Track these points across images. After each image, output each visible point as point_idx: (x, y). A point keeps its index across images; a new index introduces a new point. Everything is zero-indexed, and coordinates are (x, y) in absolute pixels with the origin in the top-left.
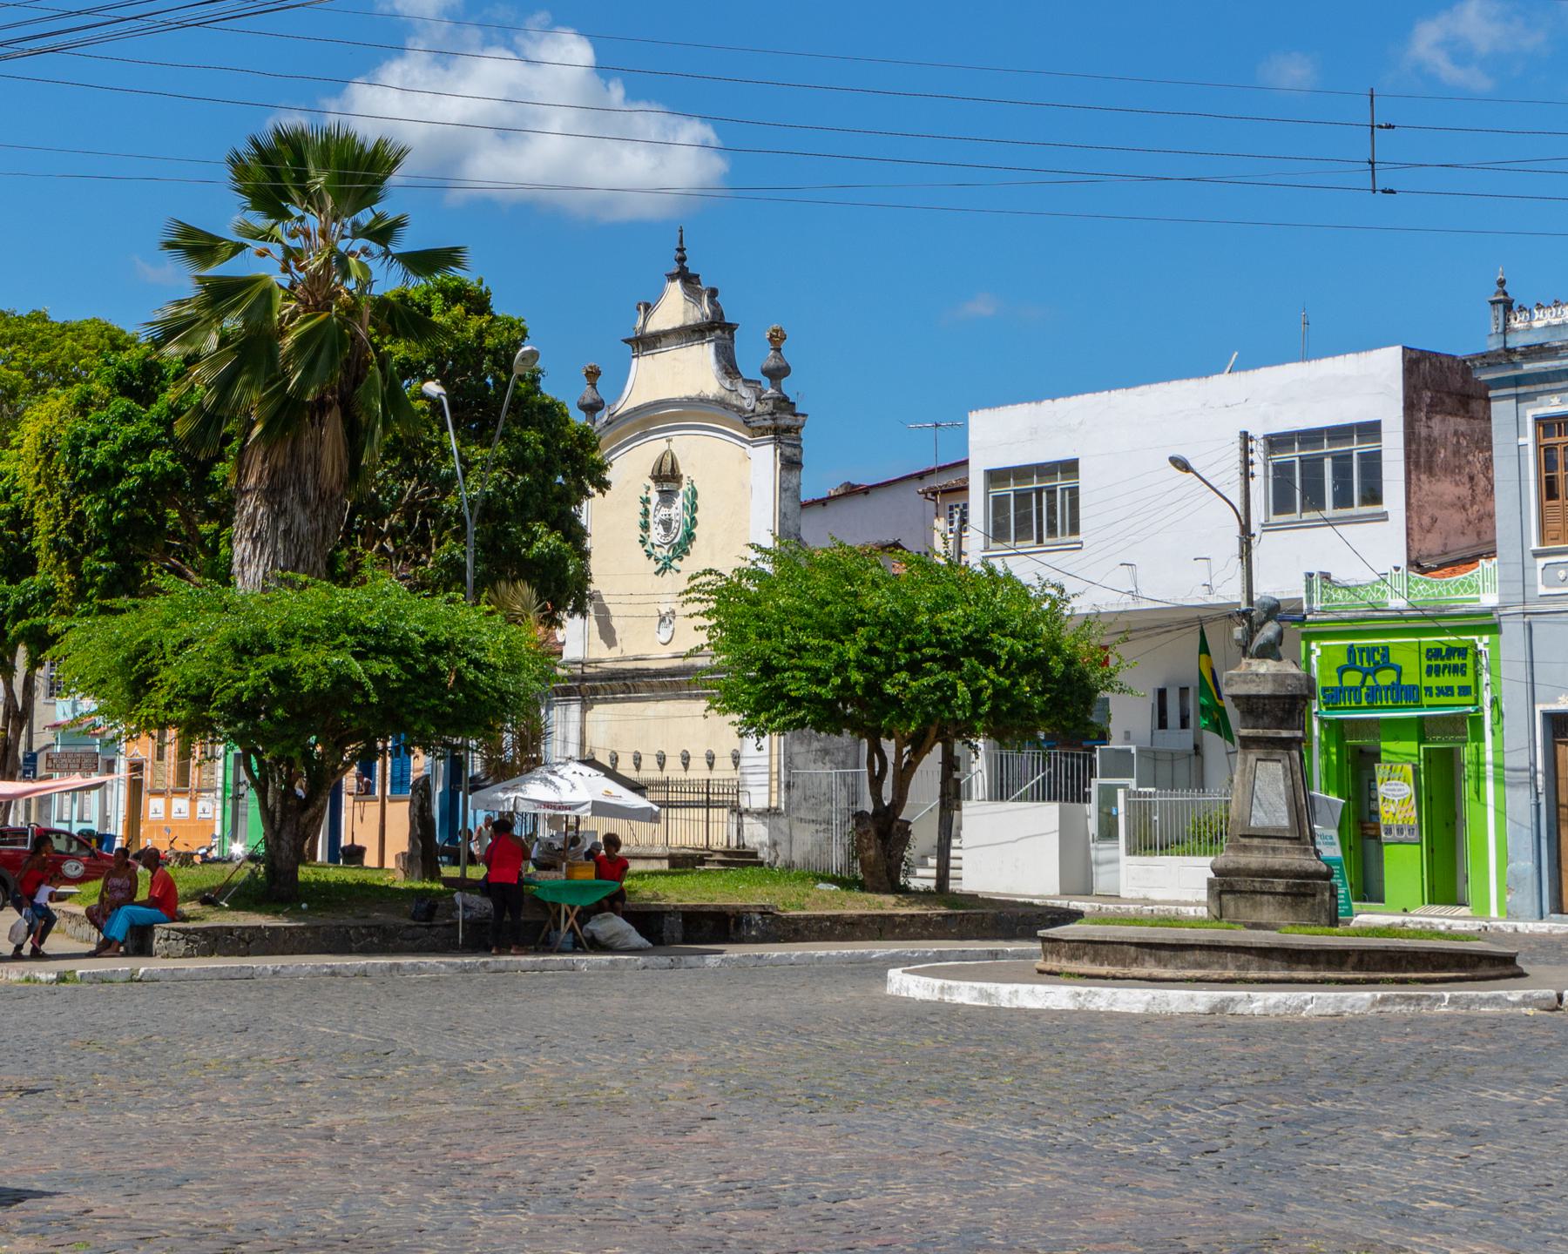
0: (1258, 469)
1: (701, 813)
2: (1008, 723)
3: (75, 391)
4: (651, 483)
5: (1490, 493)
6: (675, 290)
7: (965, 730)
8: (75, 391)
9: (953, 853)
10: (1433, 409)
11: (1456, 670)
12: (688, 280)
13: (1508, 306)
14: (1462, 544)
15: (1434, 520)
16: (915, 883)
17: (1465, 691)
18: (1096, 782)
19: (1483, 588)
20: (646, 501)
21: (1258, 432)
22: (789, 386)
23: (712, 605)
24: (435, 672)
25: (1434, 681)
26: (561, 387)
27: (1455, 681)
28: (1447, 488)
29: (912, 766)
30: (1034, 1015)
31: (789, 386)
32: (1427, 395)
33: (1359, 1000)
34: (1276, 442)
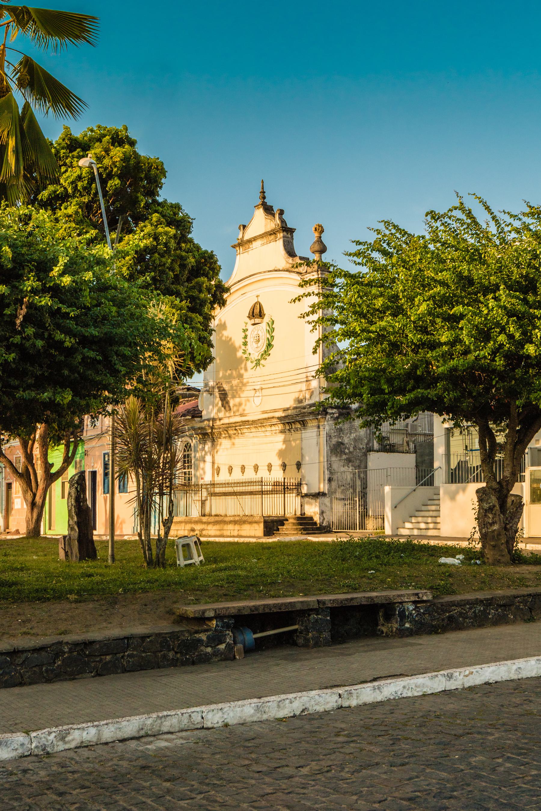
4: (248, 320)
6: (260, 213)
12: (268, 210)
20: (245, 331)
23: (315, 300)
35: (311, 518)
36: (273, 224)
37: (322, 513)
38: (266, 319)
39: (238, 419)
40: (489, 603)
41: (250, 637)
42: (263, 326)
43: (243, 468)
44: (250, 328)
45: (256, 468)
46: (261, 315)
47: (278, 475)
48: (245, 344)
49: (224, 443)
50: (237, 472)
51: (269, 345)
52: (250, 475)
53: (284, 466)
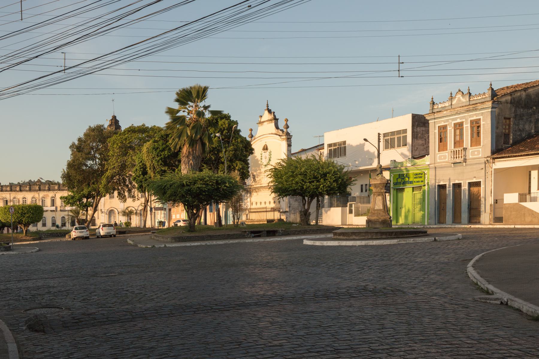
0: (382, 140)
1: (69, 65)
2: (330, 192)
3: (153, 139)
5: (429, 142)
6: (267, 112)
7: (322, 195)
8: (153, 139)
9: (159, 211)
10: (418, 126)
11: (420, 177)
12: (270, 111)
13: (434, 103)
14: (423, 153)
15: (417, 148)
16: (312, 223)
17: (422, 181)
18: (348, 204)
19: (427, 160)
21: (382, 133)
22: (289, 130)
24: (218, 188)
25: (416, 180)
26: (245, 134)
27: (420, 180)
28: (420, 142)
29: (311, 201)
30: (331, 246)
31: (289, 130)
32: (417, 123)
33: (394, 241)
34: (385, 135)
35: (283, 220)
36: (271, 117)
37: (287, 218)
38: (269, 151)
39: (259, 186)
40: (296, 231)
41: (253, 235)
42: (268, 153)
43: (261, 203)
44: (263, 153)
45: (265, 203)
46: (267, 149)
47: (273, 205)
48: (261, 159)
49: (254, 194)
50: (259, 204)
51: (270, 160)
52: (263, 205)
53: (275, 202)
